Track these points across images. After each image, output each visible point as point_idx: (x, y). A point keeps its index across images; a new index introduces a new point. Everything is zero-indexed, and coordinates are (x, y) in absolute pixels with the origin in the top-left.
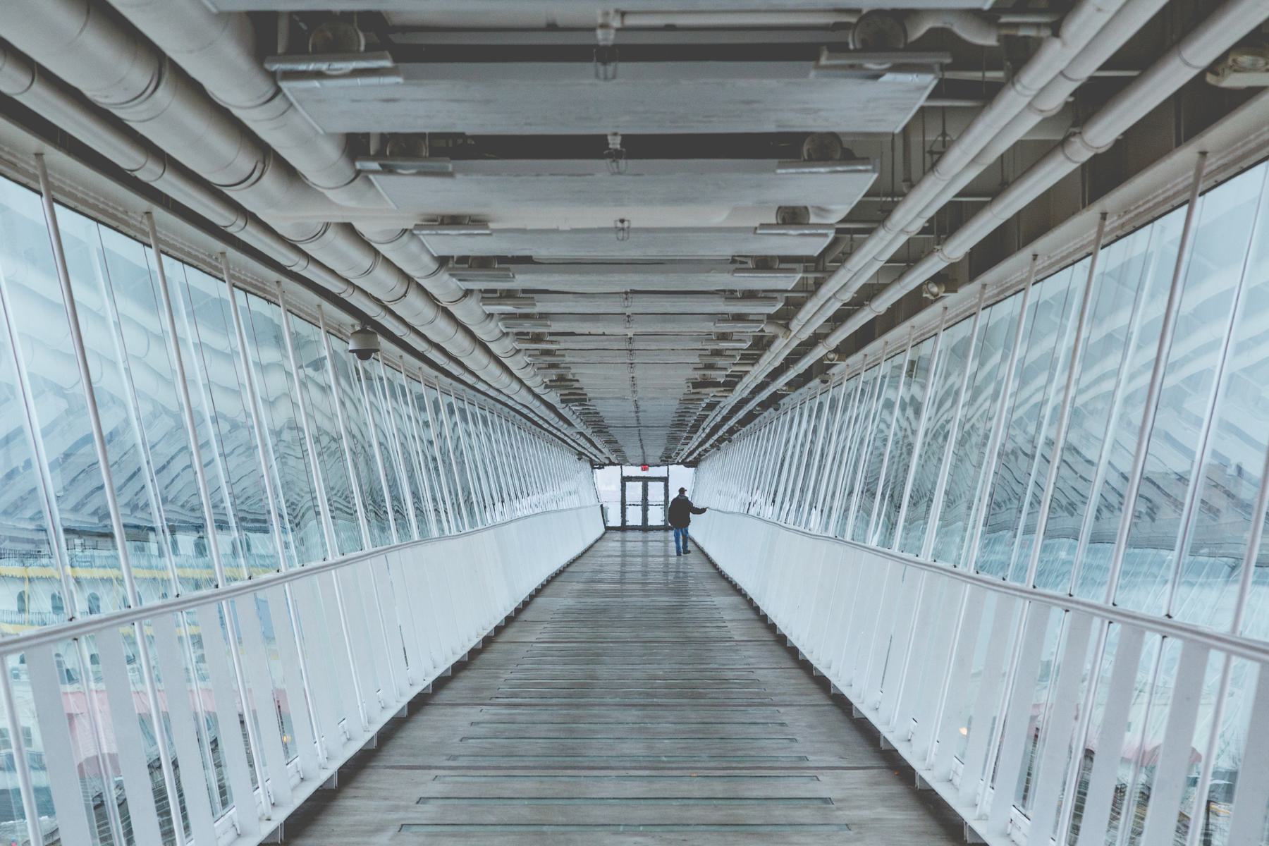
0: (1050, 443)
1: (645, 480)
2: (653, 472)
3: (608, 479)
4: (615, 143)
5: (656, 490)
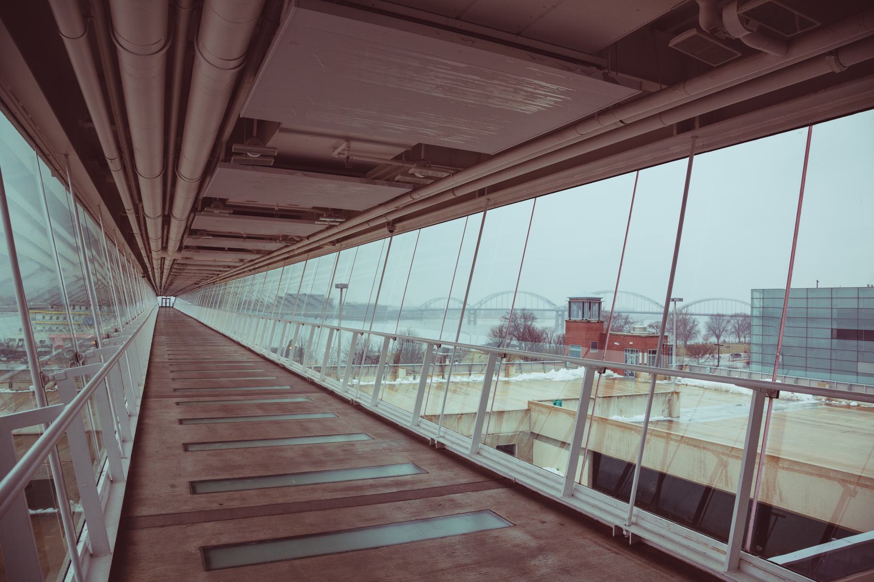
0: (240, 292)
1: (166, 299)
2: (168, 297)
3: (160, 298)
4: (226, 249)
5: (168, 301)
